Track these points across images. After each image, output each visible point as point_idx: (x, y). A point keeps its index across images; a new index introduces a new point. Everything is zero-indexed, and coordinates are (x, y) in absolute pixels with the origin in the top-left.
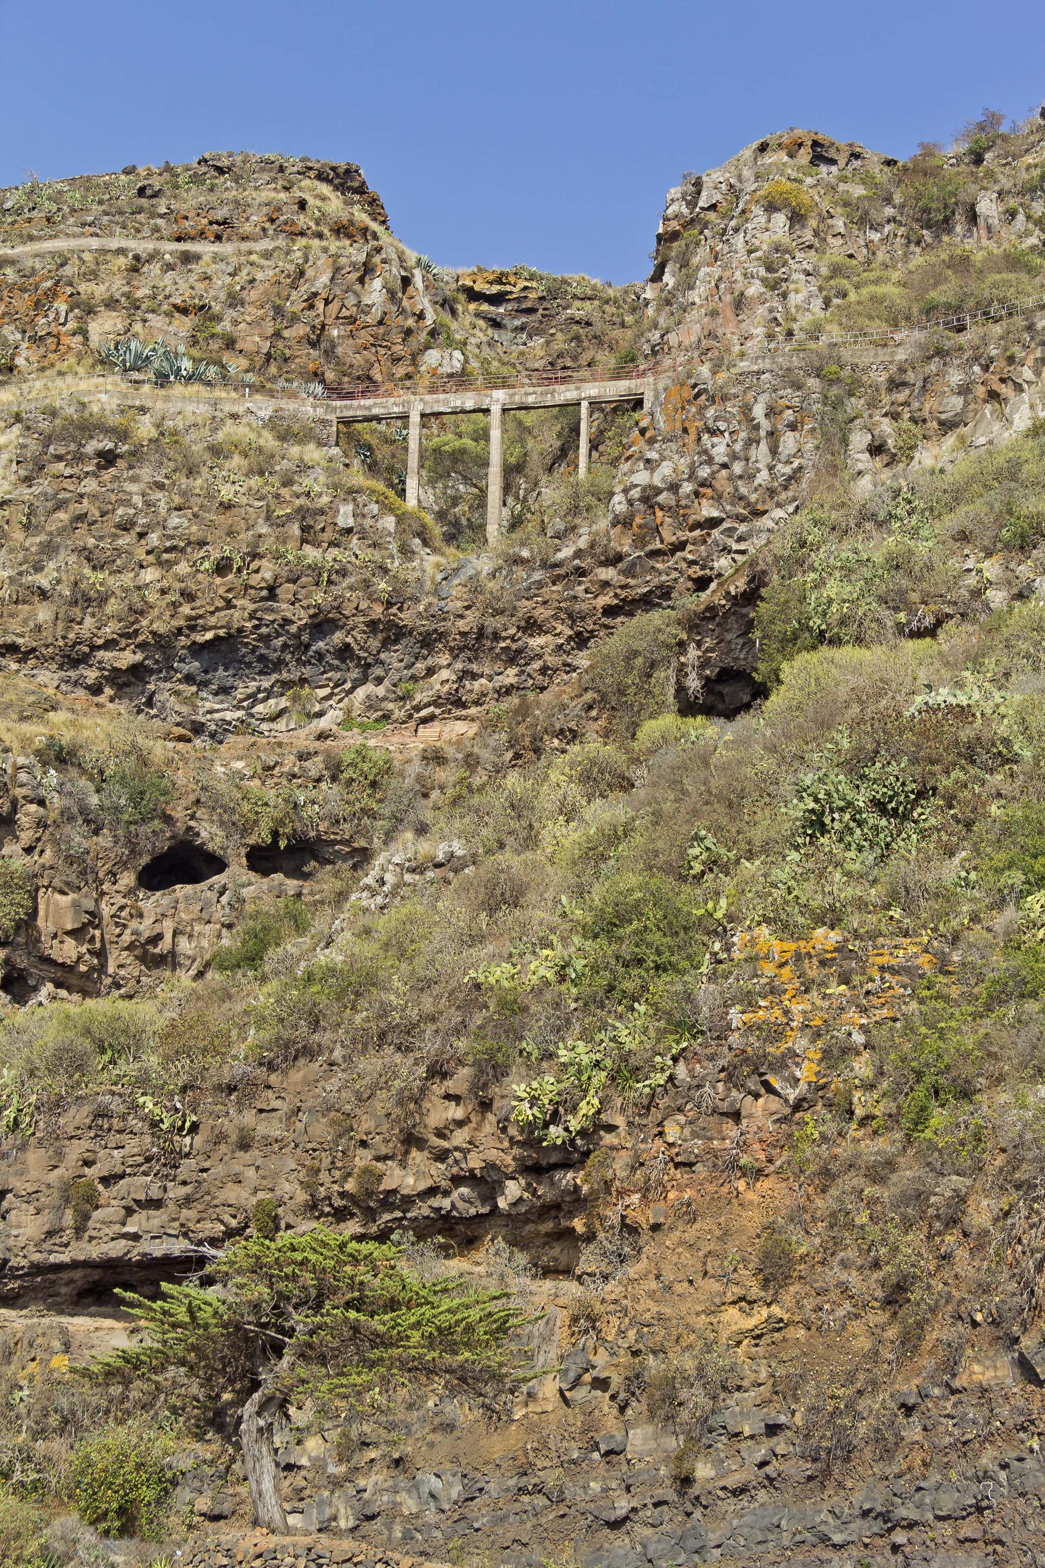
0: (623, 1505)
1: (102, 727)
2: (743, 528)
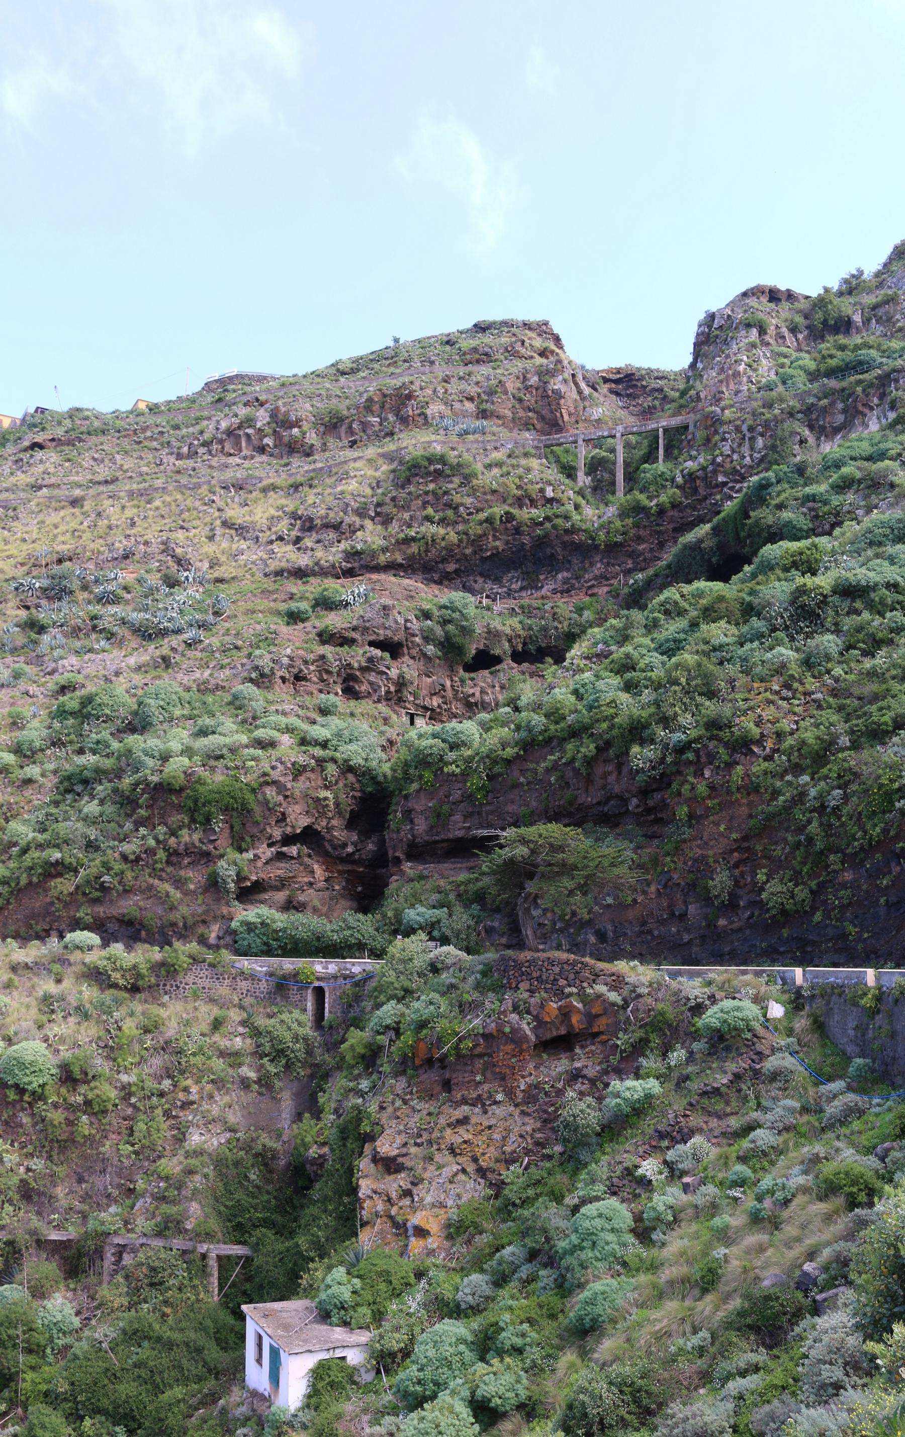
0: (686, 937)
1: (432, 596)
2: (738, 486)
